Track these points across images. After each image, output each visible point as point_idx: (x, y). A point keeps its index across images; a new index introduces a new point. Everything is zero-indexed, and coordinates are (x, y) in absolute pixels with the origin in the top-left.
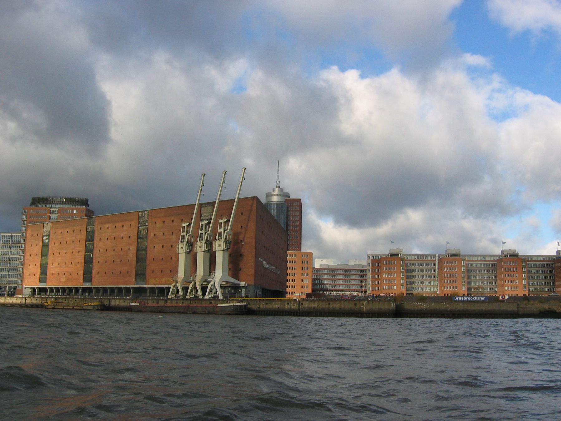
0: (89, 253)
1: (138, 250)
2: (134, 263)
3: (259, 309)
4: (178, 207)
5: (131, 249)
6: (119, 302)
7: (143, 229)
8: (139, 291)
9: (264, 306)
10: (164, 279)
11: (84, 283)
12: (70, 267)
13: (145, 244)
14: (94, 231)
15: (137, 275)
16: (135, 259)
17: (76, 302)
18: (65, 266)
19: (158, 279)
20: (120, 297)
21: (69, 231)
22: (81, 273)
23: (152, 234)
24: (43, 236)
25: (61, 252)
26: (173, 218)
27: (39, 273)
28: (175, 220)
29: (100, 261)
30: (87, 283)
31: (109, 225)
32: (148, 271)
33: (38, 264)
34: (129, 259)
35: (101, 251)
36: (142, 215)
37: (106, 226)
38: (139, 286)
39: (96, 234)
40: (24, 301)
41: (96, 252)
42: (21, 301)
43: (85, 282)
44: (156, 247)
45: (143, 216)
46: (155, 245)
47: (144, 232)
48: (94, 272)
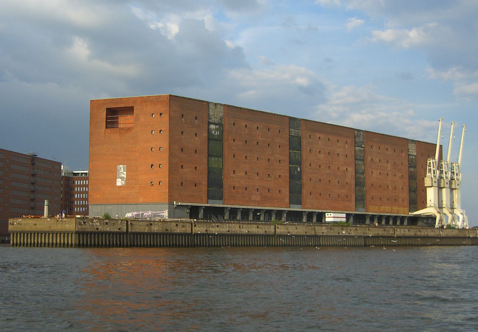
0: (294, 166)
1: (356, 172)
2: (353, 186)
3: (249, 233)
4: (305, 120)
5: (349, 169)
6: (404, 231)
7: (360, 151)
8: (295, 217)
9: (383, 232)
10: (383, 207)
11: (210, 201)
12: (267, 181)
13: (363, 167)
14: (300, 137)
15: (356, 200)
16: (353, 182)
17: (356, 231)
18: (257, 178)
19: (378, 206)
20: (409, 226)
21: (260, 127)
22: (286, 191)
23: (369, 159)
24: (209, 123)
25: (248, 155)
26: (387, 147)
27: (205, 183)
28: (389, 149)
29: (312, 179)
30: (296, 206)
31: (322, 136)
32: (368, 197)
33: (203, 168)
34: (347, 181)
35: (313, 165)
36: (357, 134)
37: (318, 135)
38: (358, 213)
39: (304, 142)
40: (273, 230)
41: (306, 167)
42: (266, 230)
43: (292, 204)
44: (374, 172)
45: (358, 136)
46: (373, 171)
47: (361, 154)
48: (304, 191)
